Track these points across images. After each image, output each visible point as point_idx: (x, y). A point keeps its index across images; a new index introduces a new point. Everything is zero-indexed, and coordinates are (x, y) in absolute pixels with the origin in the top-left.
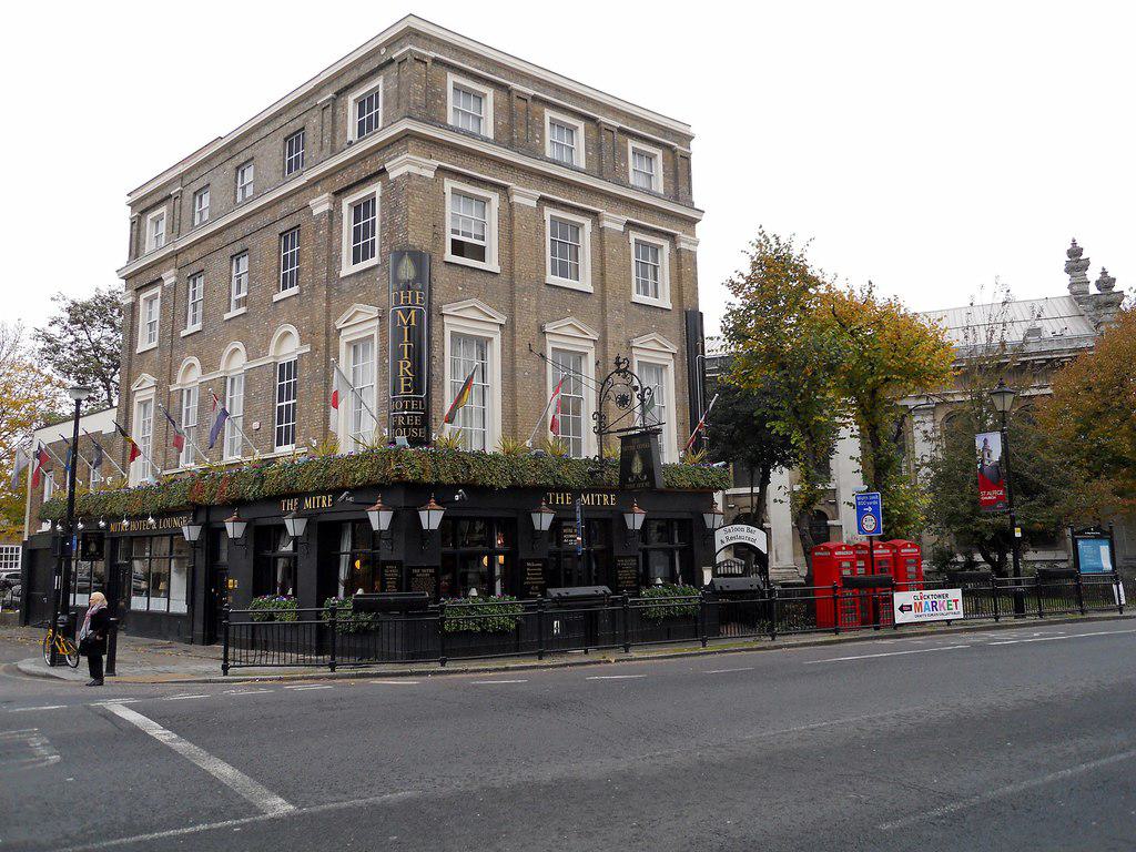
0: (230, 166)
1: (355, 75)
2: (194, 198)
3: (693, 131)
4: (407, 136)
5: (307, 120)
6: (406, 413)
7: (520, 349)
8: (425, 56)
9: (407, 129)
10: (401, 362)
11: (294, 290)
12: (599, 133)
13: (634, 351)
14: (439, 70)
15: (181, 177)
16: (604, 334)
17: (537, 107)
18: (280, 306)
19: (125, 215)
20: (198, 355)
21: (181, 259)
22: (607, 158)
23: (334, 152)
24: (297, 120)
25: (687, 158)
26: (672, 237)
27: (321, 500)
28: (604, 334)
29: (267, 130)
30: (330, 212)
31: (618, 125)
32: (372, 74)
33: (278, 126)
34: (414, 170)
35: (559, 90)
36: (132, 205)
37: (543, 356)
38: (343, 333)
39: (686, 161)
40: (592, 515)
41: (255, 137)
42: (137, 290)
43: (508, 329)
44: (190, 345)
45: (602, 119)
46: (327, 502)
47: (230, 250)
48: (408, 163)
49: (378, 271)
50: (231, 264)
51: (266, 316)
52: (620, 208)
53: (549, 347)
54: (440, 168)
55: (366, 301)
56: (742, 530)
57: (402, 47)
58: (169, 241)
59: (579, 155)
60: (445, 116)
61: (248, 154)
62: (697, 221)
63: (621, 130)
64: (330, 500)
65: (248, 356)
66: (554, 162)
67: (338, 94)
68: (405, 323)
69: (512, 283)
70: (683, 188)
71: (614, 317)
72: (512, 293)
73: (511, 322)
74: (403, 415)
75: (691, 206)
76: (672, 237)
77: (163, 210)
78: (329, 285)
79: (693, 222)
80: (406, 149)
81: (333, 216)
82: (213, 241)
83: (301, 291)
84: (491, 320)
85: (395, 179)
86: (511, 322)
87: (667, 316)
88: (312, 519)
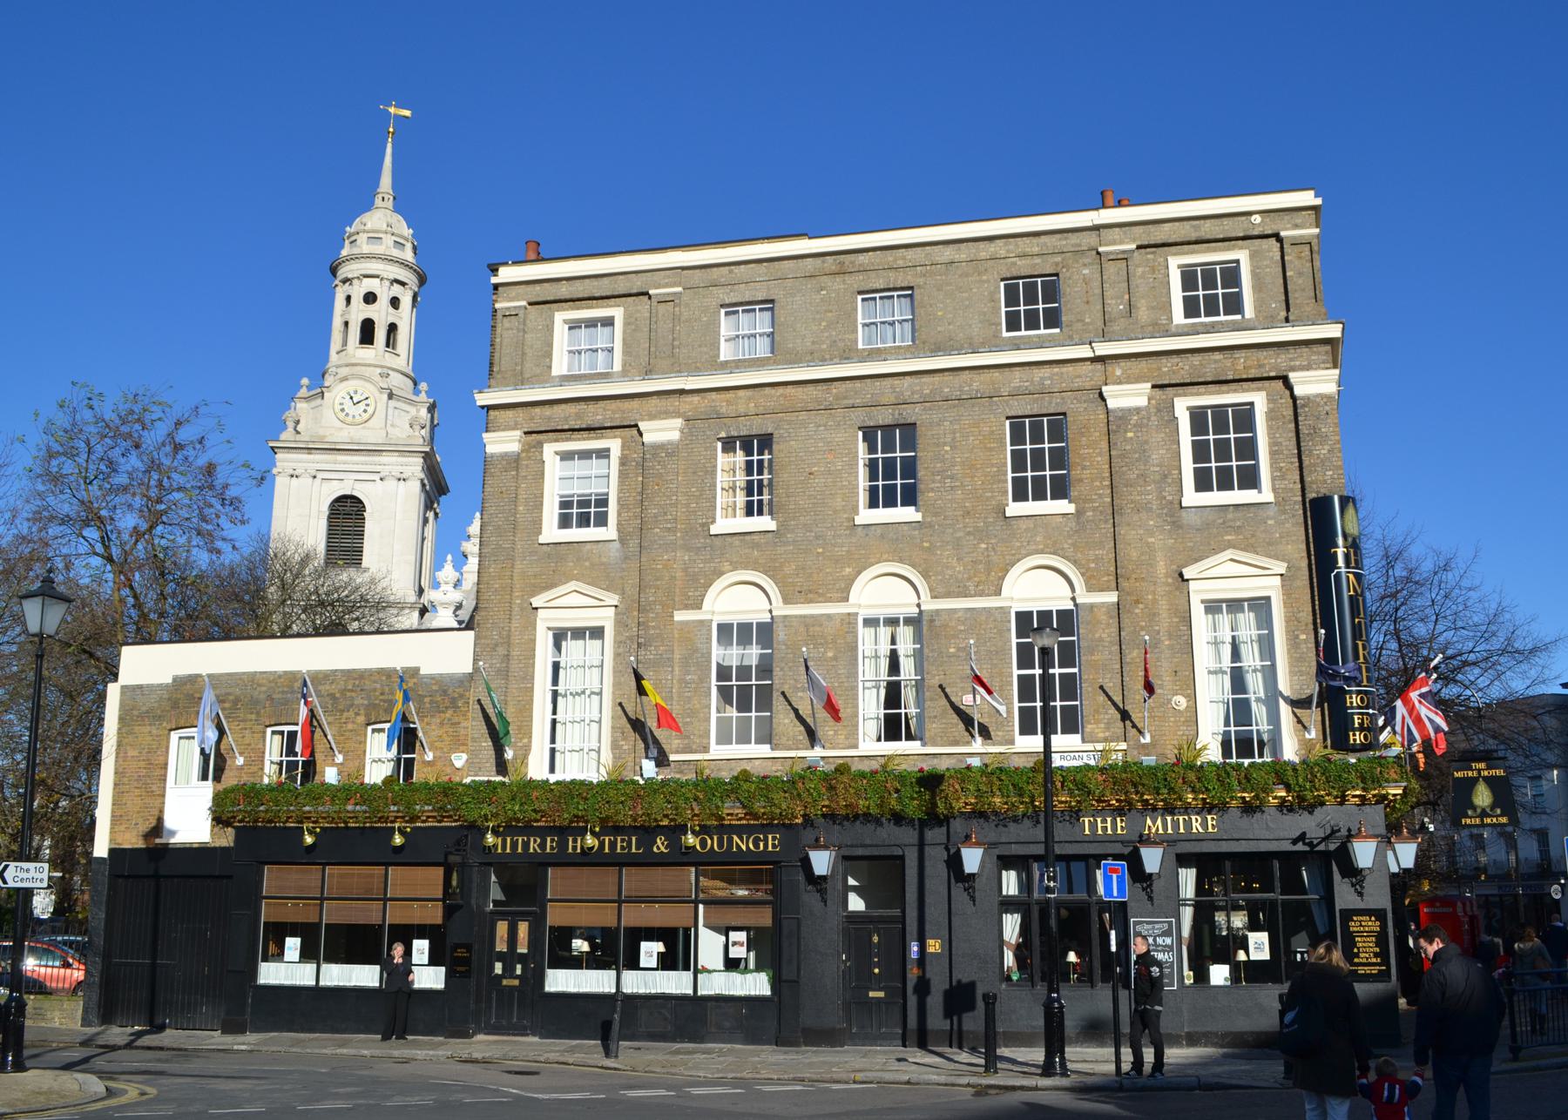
6: (1371, 711)
11: (1063, 506)
74: (1368, 714)
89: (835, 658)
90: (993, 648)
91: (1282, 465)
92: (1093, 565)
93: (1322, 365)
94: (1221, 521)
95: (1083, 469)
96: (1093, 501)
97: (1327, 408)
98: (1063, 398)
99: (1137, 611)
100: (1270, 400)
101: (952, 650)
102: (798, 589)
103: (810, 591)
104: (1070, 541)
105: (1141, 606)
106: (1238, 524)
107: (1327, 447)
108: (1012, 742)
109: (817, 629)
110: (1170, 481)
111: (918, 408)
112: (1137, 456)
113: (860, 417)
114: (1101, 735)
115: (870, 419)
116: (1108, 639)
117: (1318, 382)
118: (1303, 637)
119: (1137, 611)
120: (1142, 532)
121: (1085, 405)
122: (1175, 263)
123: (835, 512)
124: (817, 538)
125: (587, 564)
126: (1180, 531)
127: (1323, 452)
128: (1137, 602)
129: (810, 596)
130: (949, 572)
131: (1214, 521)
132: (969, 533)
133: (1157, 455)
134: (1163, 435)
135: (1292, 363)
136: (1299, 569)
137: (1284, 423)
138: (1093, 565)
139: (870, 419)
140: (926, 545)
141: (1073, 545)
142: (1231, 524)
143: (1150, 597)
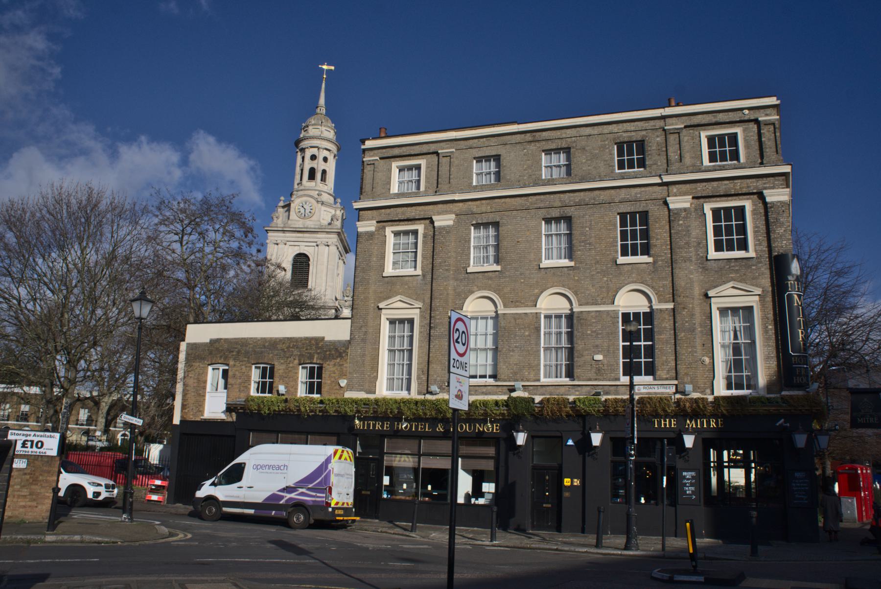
10: (800, 331)
11: (645, 259)
24: (633, 134)
33: (606, 131)
38: (383, 311)
49: (754, 261)
57: (767, 115)
68: (800, 304)
89: (529, 336)
90: (610, 331)
91: (760, 238)
92: (661, 289)
93: (781, 187)
94: (728, 267)
95: (657, 240)
96: (661, 256)
97: (783, 208)
98: (646, 204)
99: (684, 313)
100: (754, 204)
101: (589, 332)
102: (511, 300)
103: (517, 301)
104: (650, 277)
105: (686, 310)
106: (737, 268)
107: (783, 229)
108: (618, 379)
109: (520, 320)
110: (701, 246)
111: (573, 209)
112: (685, 233)
113: (543, 213)
114: (665, 377)
115: (548, 214)
116: (669, 327)
117: (779, 195)
118: (770, 327)
119: (684, 313)
120: (687, 272)
121: (658, 207)
122: (704, 135)
123: (530, 261)
124: (521, 274)
125: (406, 287)
126: (707, 272)
127: (781, 231)
128: (684, 308)
129: (517, 304)
130: (588, 292)
131: (724, 267)
132: (598, 272)
133: (695, 232)
134: (698, 222)
135: (765, 186)
136: (768, 292)
137: (761, 216)
138: (661, 289)
139: (548, 214)
140: (576, 278)
141: (652, 279)
142: (733, 268)
143: (691, 306)
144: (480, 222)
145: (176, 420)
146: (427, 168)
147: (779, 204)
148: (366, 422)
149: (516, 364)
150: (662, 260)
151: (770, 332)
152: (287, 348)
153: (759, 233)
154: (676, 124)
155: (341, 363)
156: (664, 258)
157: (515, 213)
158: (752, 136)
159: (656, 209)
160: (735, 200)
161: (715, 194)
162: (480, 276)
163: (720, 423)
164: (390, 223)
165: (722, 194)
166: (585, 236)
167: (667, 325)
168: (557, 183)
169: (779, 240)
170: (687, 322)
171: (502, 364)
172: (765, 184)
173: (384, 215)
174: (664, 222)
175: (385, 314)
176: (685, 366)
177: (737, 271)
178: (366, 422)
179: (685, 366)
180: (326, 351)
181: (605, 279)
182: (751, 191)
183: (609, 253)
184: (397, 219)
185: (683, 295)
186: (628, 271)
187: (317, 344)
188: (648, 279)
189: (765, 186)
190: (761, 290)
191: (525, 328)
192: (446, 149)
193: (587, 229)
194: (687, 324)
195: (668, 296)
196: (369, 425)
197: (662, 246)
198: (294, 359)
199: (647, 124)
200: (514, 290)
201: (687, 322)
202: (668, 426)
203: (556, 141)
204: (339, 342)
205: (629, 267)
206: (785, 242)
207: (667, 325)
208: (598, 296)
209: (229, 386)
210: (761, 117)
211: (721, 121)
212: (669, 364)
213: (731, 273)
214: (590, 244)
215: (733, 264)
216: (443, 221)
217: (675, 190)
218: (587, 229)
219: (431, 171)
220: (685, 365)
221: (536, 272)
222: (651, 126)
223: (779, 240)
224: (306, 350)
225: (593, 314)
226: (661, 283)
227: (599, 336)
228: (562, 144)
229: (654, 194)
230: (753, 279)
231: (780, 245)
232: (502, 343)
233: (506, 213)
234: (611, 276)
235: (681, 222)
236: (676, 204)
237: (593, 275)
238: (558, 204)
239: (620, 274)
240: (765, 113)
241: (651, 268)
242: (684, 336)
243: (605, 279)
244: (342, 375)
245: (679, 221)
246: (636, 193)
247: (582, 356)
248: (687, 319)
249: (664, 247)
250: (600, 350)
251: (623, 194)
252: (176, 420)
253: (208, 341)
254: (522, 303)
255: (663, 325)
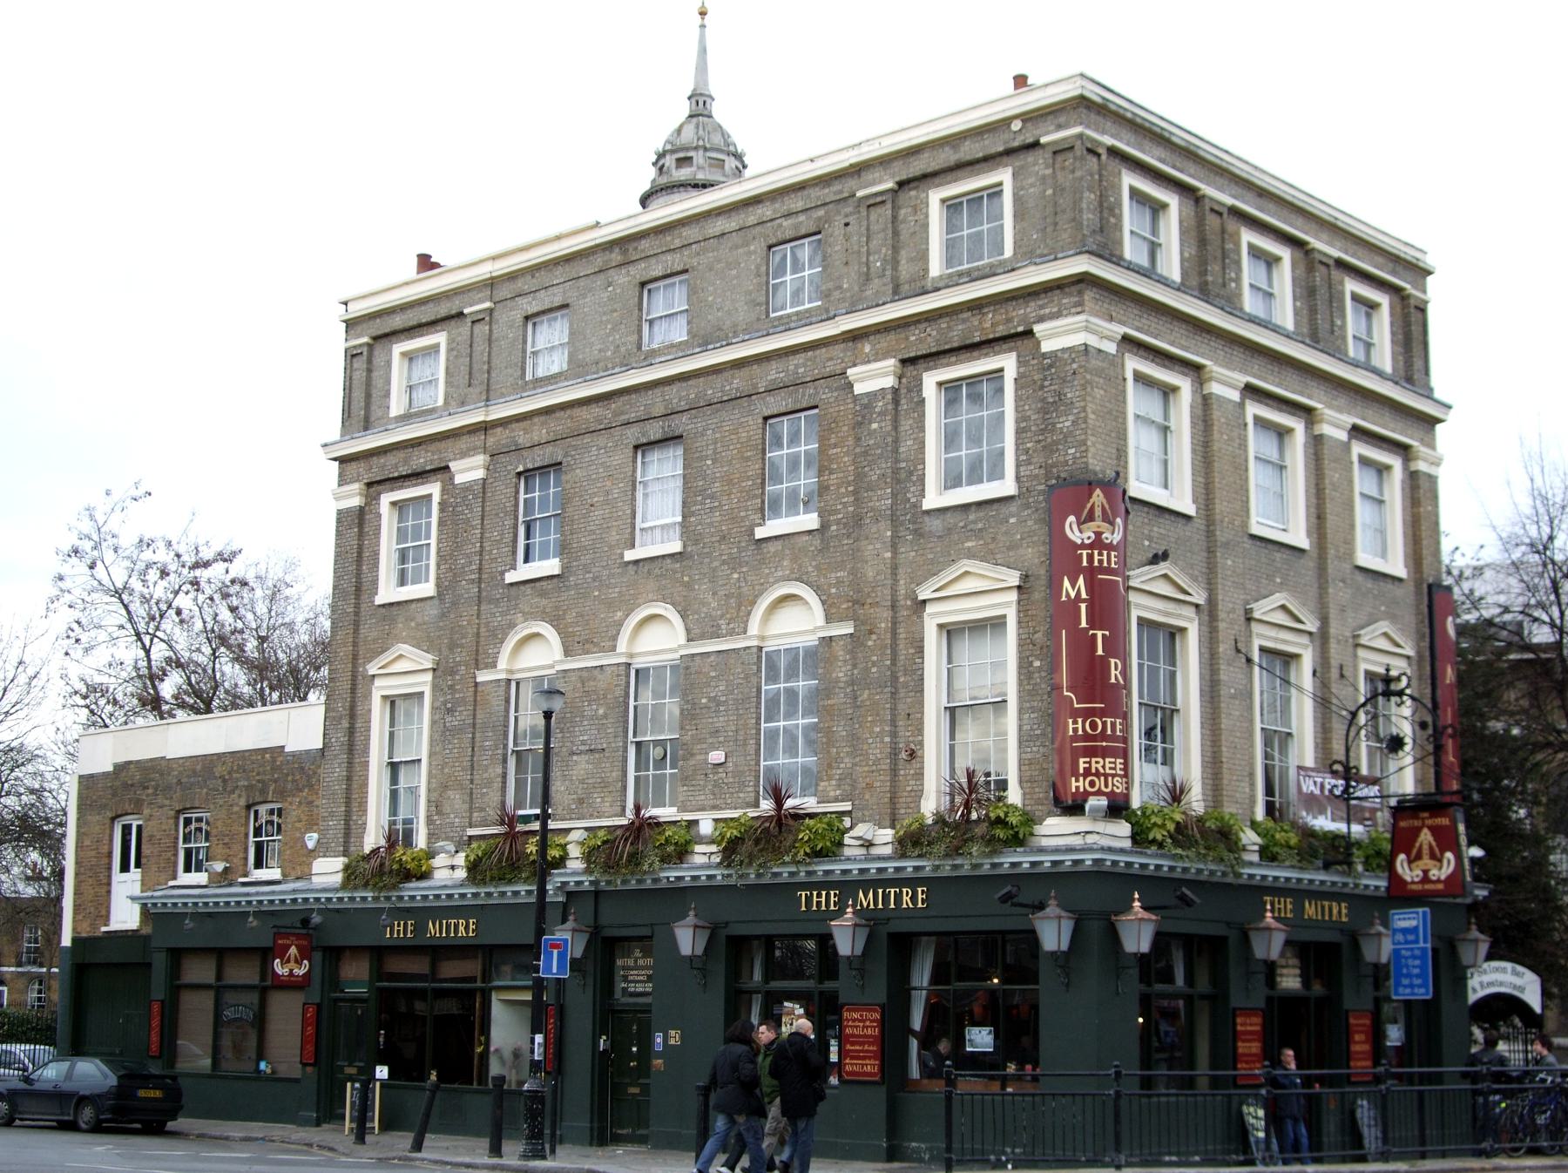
0: (624, 279)
1: (947, 157)
2: (525, 325)
3: (1429, 261)
4: (1084, 280)
5: (828, 220)
7: (1224, 648)
8: (1100, 144)
9: (1086, 273)
12: (1310, 268)
13: (1361, 653)
14: (1114, 164)
15: (491, 283)
16: (1324, 621)
17: (1231, 224)
18: (772, 548)
19: (335, 344)
20: (556, 621)
21: (497, 438)
22: (1321, 306)
23: (898, 294)
24: (802, 218)
25: (1422, 310)
26: (1403, 450)
27: (456, 926)
28: (1324, 621)
29: (721, 225)
30: (895, 391)
31: (1336, 253)
32: (988, 161)
33: (752, 220)
34: (1093, 341)
35: (1263, 194)
36: (351, 325)
37: (1249, 661)
38: (929, 609)
39: (1419, 315)
40: (1306, 936)
41: (691, 233)
42: (369, 485)
43: (1209, 613)
44: (529, 598)
45: (1314, 243)
46: (467, 928)
47: (633, 435)
48: (1087, 329)
50: (635, 461)
51: (734, 563)
52: (1342, 401)
53: (1257, 643)
54: (1126, 339)
55: (988, 556)
56: (1504, 970)
57: (1060, 127)
58: (455, 400)
59: (1283, 305)
60: (1120, 243)
61: (674, 262)
62: (1439, 421)
63: (1340, 264)
64: (472, 927)
65: (688, 630)
66: (1252, 320)
67: (901, 184)
69: (1210, 533)
70: (1418, 364)
71: (1338, 594)
72: (1210, 552)
73: (1212, 601)
75: (1428, 394)
76: (1403, 450)
77: (440, 338)
78: (895, 521)
79: (1431, 422)
80: (1080, 304)
81: (904, 398)
82: (584, 413)
83: (824, 527)
84: (1188, 598)
85: (1053, 355)
86: (1212, 601)
87: (1399, 591)
88: (871, 921)
89: (605, 716)
92: (833, 591)
93: (1073, 310)
95: (830, 474)
96: (837, 512)
99: (870, 643)
104: (814, 563)
105: (874, 637)
106: (980, 526)
107: (1071, 418)
111: (685, 418)
115: (643, 435)
118: (1037, 664)
119: (870, 643)
123: (611, 547)
125: (413, 624)
127: (1067, 424)
130: (705, 610)
135: (1042, 312)
140: (686, 579)
141: (817, 568)
144: (530, 466)
145: (66, 941)
146: (450, 350)
147: (1066, 356)
148: (880, 891)
149: (582, 782)
150: (838, 522)
151: (1037, 675)
152: (229, 773)
153: (1029, 434)
154: (881, 182)
155: (310, 798)
156: (840, 516)
157: (587, 439)
158: (1032, 185)
159: (831, 400)
160: (986, 355)
161: (942, 348)
162: (528, 589)
163: (920, 896)
164: (388, 485)
165: (955, 345)
166: (704, 479)
167: (841, 675)
168: (814, 319)
169: (1061, 447)
170: (874, 664)
171: (558, 783)
172: (1041, 307)
173: (377, 469)
174: (846, 428)
175: (933, 615)
176: (866, 769)
177: (978, 534)
178: (880, 891)
179: (866, 769)
180: (287, 775)
181: (736, 576)
182: (1013, 331)
183: (742, 514)
184: (396, 474)
185: (869, 601)
186: (775, 554)
187: (274, 760)
188: (810, 569)
189: (1042, 312)
190: (1017, 574)
191: (599, 699)
192: (477, 303)
193: (709, 462)
194: (874, 670)
195: (844, 606)
196: (886, 897)
197: (839, 486)
198: (240, 796)
199: (827, 191)
200: (582, 616)
201: (874, 664)
202: (823, 908)
203: (663, 257)
204: (308, 752)
205: (778, 545)
206: (1073, 451)
207: (841, 675)
208: (722, 616)
209: (144, 861)
210: (1047, 133)
211: (969, 158)
212: (842, 765)
213: (968, 539)
214: (712, 497)
215: (972, 517)
216: (469, 470)
217: (867, 348)
218: (709, 462)
219: (456, 357)
220: (867, 765)
221: (619, 570)
222: (835, 193)
223: (1061, 447)
224: (258, 774)
225: (712, 658)
226: (833, 575)
227: (722, 708)
228: (673, 265)
229: (829, 363)
230: (1009, 548)
231: (1061, 458)
232: (560, 735)
233: (573, 442)
234: (744, 569)
235: (875, 426)
236: (866, 383)
237: (714, 570)
238: (659, 410)
239: (762, 562)
240: (1056, 122)
241: (817, 542)
242: (869, 699)
243: (736, 576)
244: (311, 825)
245: (870, 423)
246: (797, 366)
247: (692, 755)
248: (875, 658)
249: (843, 490)
250: (721, 739)
251: (774, 373)
252: (66, 941)
253: (110, 768)
254: (596, 645)
255: (834, 675)
